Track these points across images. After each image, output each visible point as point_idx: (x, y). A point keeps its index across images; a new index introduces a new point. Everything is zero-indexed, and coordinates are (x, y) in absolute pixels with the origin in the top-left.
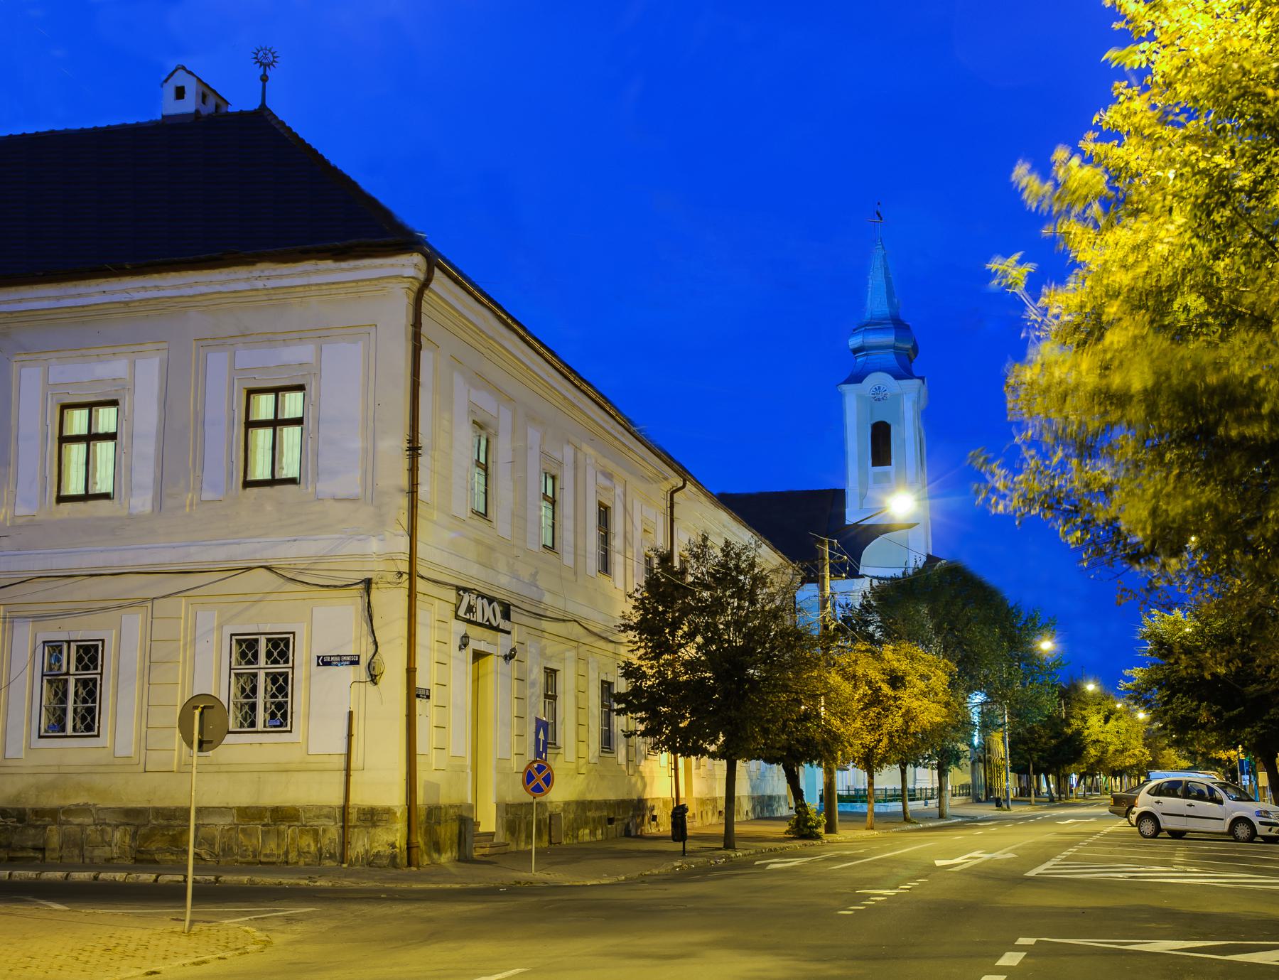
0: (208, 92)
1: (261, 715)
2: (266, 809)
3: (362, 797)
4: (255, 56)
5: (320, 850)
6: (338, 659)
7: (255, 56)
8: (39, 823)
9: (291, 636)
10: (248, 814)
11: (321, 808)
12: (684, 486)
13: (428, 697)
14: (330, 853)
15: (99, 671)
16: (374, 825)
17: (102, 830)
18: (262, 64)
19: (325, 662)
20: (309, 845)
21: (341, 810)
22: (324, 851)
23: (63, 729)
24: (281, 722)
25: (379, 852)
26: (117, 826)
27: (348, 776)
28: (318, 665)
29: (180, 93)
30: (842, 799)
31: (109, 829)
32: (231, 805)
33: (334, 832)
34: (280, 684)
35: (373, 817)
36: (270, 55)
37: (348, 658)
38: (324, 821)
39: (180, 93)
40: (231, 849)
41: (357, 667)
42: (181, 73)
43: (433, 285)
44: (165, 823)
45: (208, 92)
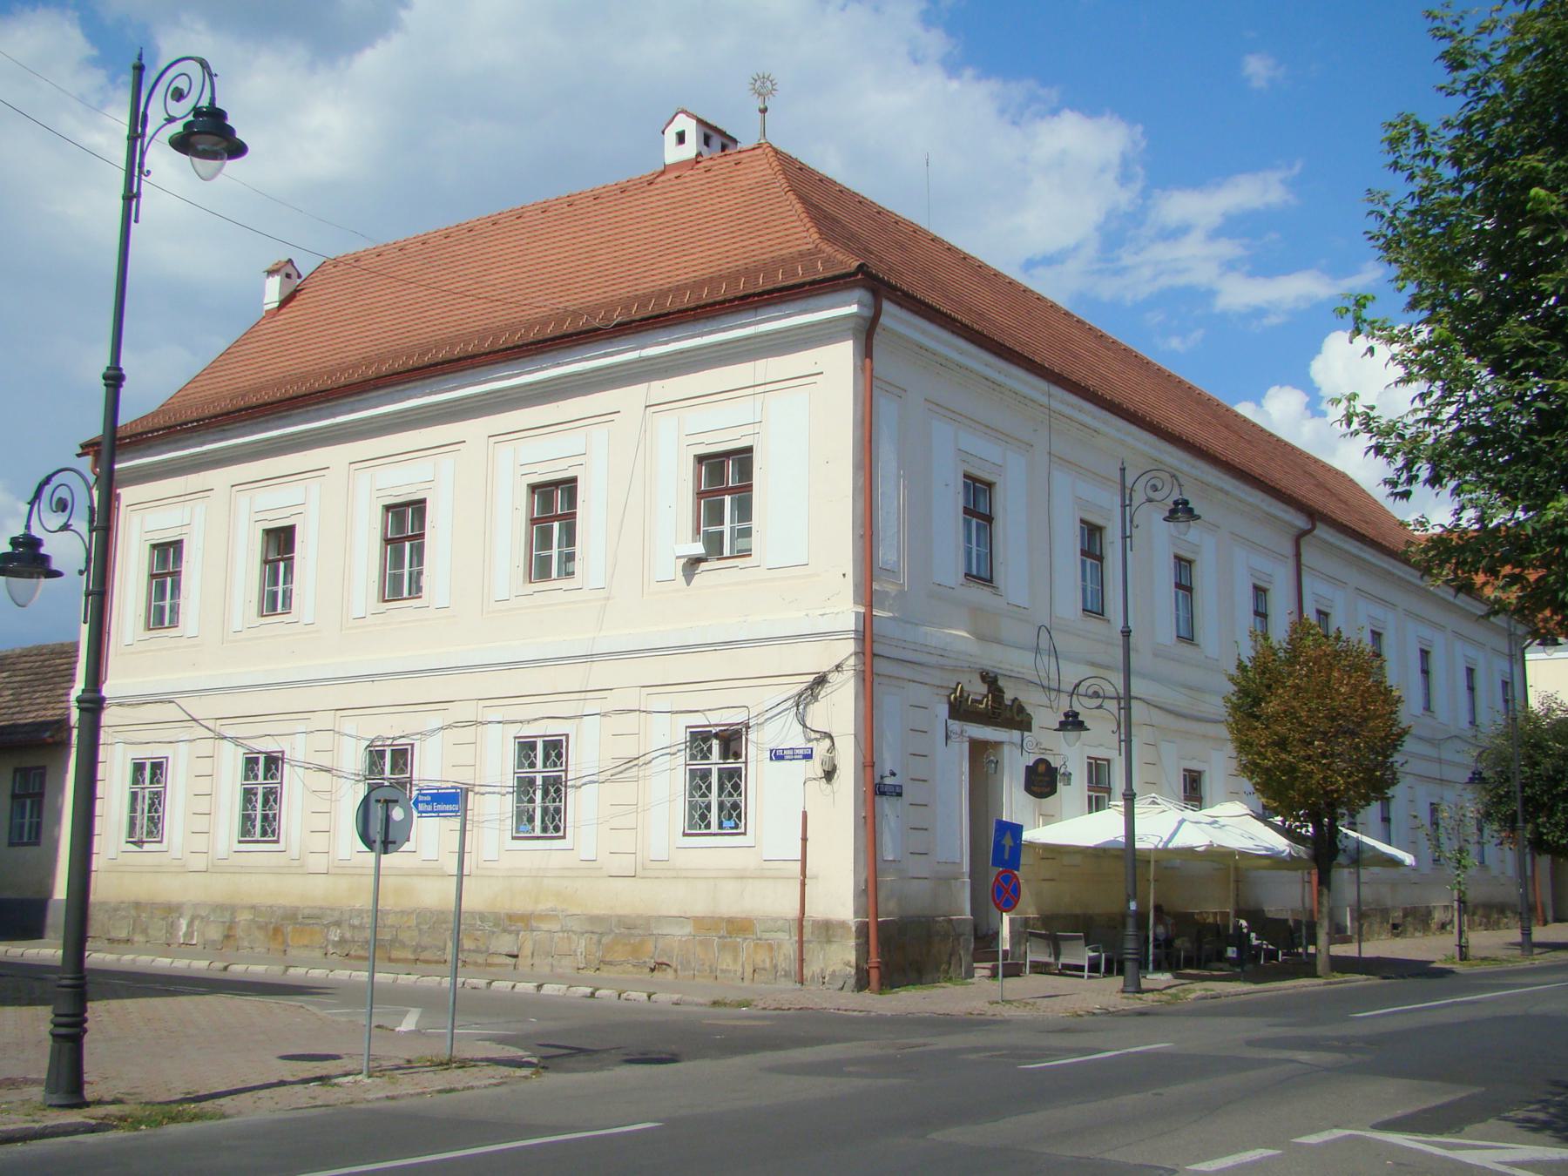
0: (710, 132)
1: (714, 816)
2: (721, 919)
3: (816, 911)
4: (752, 86)
5: (775, 966)
6: (791, 752)
7: (752, 86)
8: (513, 928)
9: (164, 760)
10: (706, 925)
11: (775, 920)
12: (1314, 528)
13: (900, 795)
14: (786, 971)
15: (564, 768)
16: (829, 941)
17: (569, 938)
18: (760, 94)
19: (777, 756)
20: (764, 961)
21: (797, 922)
22: (779, 968)
23: (708, 826)
24: (736, 823)
25: (834, 971)
26: (582, 934)
27: (803, 885)
28: (771, 759)
29: (681, 138)
30: (366, 959)
31: (574, 937)
32: (688, 915)
33: (789, 946)
34: (732, 779)
35: (828, 929)
36: (768, 84)
37: (801, 752)
38: (780, 935)
39: (681, 138)
40: (689, 962)
41: (810, 762)
42: (681, 117)
43: (883, 320)
44: (626, 931)
45: (710, 132)
